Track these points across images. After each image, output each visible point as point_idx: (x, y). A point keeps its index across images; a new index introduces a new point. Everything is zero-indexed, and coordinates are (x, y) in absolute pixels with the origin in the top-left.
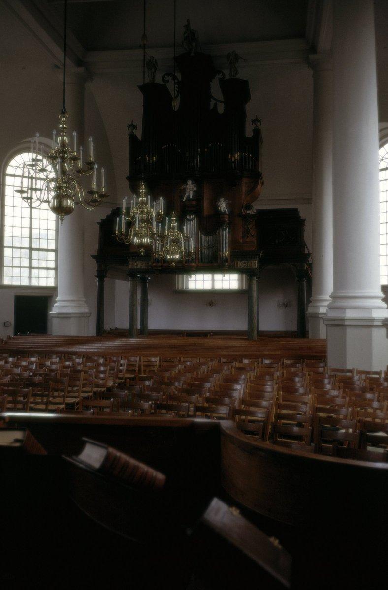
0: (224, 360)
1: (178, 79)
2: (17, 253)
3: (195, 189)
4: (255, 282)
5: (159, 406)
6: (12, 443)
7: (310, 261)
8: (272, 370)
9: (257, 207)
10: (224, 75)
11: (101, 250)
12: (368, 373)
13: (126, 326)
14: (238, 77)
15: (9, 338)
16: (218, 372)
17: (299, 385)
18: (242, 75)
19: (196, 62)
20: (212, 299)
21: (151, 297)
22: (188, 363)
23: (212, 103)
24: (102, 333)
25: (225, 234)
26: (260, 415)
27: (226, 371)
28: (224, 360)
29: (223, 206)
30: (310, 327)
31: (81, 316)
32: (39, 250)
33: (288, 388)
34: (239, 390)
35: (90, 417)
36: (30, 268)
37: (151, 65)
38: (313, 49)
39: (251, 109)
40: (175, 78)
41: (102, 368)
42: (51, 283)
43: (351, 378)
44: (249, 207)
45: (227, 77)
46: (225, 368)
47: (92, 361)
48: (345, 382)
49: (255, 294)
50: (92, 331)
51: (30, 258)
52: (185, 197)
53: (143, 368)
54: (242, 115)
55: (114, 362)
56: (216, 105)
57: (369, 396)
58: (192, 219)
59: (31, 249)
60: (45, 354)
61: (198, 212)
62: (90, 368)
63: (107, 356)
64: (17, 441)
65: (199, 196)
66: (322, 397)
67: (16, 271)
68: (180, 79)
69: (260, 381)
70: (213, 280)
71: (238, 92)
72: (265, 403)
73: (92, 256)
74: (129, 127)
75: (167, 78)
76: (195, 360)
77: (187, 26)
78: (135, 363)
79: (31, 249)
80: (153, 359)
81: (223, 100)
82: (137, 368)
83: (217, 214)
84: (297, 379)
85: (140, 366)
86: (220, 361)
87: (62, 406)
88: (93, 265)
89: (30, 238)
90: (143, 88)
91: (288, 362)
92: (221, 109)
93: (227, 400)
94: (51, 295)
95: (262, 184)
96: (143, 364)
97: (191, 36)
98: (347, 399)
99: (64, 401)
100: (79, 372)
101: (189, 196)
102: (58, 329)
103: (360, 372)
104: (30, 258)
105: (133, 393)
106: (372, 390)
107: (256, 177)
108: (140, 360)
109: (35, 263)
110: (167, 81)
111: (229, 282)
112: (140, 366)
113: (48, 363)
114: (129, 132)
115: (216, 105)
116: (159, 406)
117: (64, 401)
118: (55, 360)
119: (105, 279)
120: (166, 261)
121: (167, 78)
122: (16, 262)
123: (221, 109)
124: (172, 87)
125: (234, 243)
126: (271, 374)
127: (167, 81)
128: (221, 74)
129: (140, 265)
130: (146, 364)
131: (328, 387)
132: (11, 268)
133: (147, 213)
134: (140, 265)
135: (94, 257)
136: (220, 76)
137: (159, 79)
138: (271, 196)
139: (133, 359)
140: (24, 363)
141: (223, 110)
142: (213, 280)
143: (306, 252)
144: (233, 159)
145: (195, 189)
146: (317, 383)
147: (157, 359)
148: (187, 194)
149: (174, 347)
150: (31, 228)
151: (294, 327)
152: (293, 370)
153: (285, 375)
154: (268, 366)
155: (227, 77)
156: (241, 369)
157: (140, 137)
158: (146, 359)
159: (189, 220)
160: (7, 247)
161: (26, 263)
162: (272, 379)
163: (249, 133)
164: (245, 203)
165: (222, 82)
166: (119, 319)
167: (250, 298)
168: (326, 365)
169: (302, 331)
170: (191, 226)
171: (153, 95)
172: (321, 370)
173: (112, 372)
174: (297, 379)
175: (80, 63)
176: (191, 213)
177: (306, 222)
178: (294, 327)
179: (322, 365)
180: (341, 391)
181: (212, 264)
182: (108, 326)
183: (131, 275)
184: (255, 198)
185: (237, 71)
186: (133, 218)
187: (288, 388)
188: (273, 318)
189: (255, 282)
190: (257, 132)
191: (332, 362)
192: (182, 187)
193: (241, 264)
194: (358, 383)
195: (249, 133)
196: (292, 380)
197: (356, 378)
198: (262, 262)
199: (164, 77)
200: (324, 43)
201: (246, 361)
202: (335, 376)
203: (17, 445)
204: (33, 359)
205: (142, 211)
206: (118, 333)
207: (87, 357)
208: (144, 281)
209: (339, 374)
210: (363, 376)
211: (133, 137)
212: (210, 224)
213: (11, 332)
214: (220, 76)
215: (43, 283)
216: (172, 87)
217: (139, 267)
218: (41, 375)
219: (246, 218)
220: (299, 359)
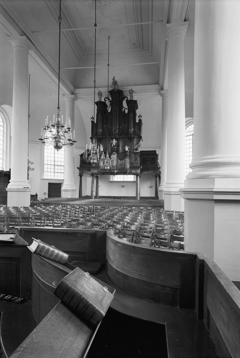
0: (126, 207)
1: (110, 100)
2: (49, 166)
3: (116, 142)
4: (139, 178)
5: (94, 225)
6: (9, 239)
7: (160, 170)
8: (143, 211)
9: (140, 150)
10: (128, 98)
11: (80, 166)
12: (179, 212)
13: (89, 194)
14: (133, 99)
15: (45, 198)
16: (121, 212)
17: (151, 216)
18: (135, 98)
19: (117, 94)
20: (123, 184)
21: (100, 184)
22: (111, 208)
23: (124, 109)
24: (81, 197)
25: (127, 160)
26: (133, 228)
27: (125, 211)
28: (126, 207)
29: (127, 149)
30: (159, 195)
31: (73, 191)
32: (58, 166)
33: (147, 218)
34: (128, 219)
35: (81, 229)
36: (54, 172)
37: (100, 94)
38: (162, 89)
39: (138, 112)
40: (109, 99)
41: (77, 210)
42: (62, 178)
43: (172, 214)
44: (137, 149)
45: (129, 99)
46: (125, 210)
47: (74, 207)
48: (170, 216)
49: (139, 182)
50: (77, 196)
51: (54, 169)
52: (113, 145)
53: (94, 210)
54: (135, 114)
55: (83, 208)
56: (124, 110)
57: (178, 221)
58: (115, 154)
59: (55, 165)
60: (57, 204)
61: (117, 151)
62: (73, 210)
63: (80, 206)
64: (11, 238)
65: (118, 145)
66: (160, 222)
67: (49, 174)
68: (111, 100)
69: (137, 215)
70: (124, 177)
71: (133, 105)
72: (136, 224)
73: (77, 168)
74: (91, 118)
75: (106, 99)
76: (114, 207)
77: (114, 79)
78: (91, 208)
79: (55, 165)
80: (98, 207)
81: (127, 108)
82: (92, 210)
83: (125, 152)
84: (151, 214)
85: (93, 209)
86: (124, 208)
87: (59, 224)
88: (78, 171)
89: (54, 161)
90: (96, 103)
91: (149, 208)
92: (126, 111)
93: (121, 222)
94: (62, 183)
95: (142, 141)
96: (94, 208)
97: (115, 83)
98: (169, 222)
99: (61, 222)
100: (68, 211)
101: (114, 145)
102: (65, 195)
103: (176, 212)
104: (54, 169)
105: (86, 219)
106: (180, 219)
107: (140, 138)
108: (93, 207)
109: (56, 171)
110: (106, 101)
111: (131, 178)
112: (93, 209)
113: (57, 208)
114: (91, 120)
115: (124, 110)
116: (94, 225)
117: (61, 222)
118: (60, 206)
119: (82, 177)
120: (105, 170)
121: (106, 99)
122: (49, 170)
123: (126, 111)
124: (108, 103)
125: (131, 163)
126: (142, 213)
127: (106, 101)
128: (127, 98)
129: (95, 171)
130: (95, 208)
131: (163, 217)
132: (50, 173)
133: (96, 150)
134: (95, 171)
135: (78, 168)
136: (126, 99)
137: (103, 100)
138: (145, 145)
139: (90, 207)
140: (47, 208)
141: (191, 158)
142: (124, 177)
143: (159, 167)
144: (131, 131)
145: (116, 142)
146: (159, 216)
147: (100, 207)
148: (113, 144)
149: (107, 202)
150: (54, 157)
151: (154, 195)
152: (150, 211)
153: (147, 213)
154: (142, 209)
155: (129, 99)
156: (131, 211)
157: (95, 122)
158: (95, 207)
159: (114, 154)
160: (45, 164)
161: (53, 170)
162: (141, 215)
163: (137, 121)
164: (135, 148)
165: (127, 101)
166: (87, 192)
167: (137, 184)
168: (164, 209)
169: (157, 197)
170: (114, 156)
171: (101, 106)
172: (161, 211)
173: (81, 211)
174: (151, 214)
175: (72, 93)
176: (114, 152)
177: (159, 156)
178: (154, 195)
179: (162, 209)
180: (167, 219)
181: (123, 172)
182: (83, 195)
183: (92, 175)
184: (139, 146)
185: (133, 97)
186: (90, 152)
187: (147, 218)
188: (146, 191)
189: (139, 178)
190: (140, 120)
191: (166, 208)
192: (111, 142)
193: (134, 171)
194: (174, 216)
195: (137, 121)
196: (150, 215)
197: (174, 214)
198: (142, 171)
199: (105, 99)
200: (166, 86)
201: (133, 208)
202: (166, 213)
203: (11, 240)
204: (51, 207)
205: (94, 150)
206: (87, 197)
207: (73, 206)
208: (97, 177)
209: (168, 212)
210: (177, 214)
211: (93, 122)
212: (122, 156)
213: (47, 197)
214: (126, 99)
215: (59, 178)
216: (108, 103)
217: (95, 172)
218: (52, 212)
219: (136, 154)
220: (154, 207)
